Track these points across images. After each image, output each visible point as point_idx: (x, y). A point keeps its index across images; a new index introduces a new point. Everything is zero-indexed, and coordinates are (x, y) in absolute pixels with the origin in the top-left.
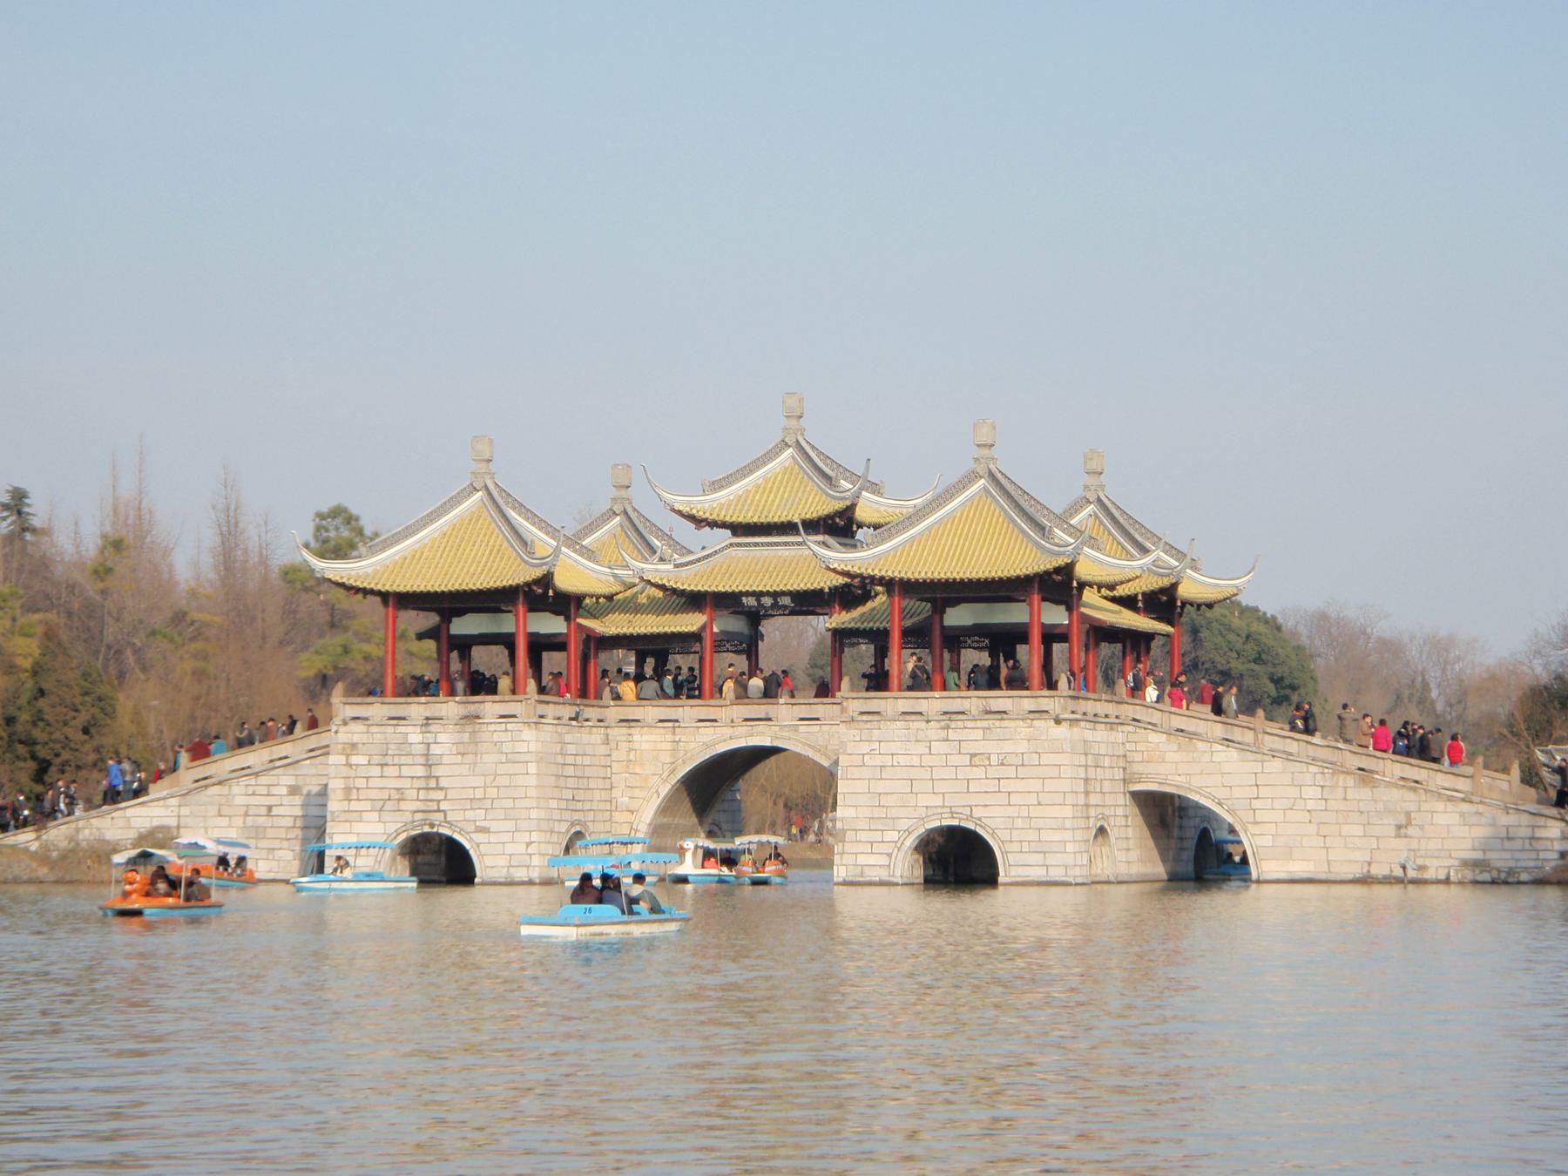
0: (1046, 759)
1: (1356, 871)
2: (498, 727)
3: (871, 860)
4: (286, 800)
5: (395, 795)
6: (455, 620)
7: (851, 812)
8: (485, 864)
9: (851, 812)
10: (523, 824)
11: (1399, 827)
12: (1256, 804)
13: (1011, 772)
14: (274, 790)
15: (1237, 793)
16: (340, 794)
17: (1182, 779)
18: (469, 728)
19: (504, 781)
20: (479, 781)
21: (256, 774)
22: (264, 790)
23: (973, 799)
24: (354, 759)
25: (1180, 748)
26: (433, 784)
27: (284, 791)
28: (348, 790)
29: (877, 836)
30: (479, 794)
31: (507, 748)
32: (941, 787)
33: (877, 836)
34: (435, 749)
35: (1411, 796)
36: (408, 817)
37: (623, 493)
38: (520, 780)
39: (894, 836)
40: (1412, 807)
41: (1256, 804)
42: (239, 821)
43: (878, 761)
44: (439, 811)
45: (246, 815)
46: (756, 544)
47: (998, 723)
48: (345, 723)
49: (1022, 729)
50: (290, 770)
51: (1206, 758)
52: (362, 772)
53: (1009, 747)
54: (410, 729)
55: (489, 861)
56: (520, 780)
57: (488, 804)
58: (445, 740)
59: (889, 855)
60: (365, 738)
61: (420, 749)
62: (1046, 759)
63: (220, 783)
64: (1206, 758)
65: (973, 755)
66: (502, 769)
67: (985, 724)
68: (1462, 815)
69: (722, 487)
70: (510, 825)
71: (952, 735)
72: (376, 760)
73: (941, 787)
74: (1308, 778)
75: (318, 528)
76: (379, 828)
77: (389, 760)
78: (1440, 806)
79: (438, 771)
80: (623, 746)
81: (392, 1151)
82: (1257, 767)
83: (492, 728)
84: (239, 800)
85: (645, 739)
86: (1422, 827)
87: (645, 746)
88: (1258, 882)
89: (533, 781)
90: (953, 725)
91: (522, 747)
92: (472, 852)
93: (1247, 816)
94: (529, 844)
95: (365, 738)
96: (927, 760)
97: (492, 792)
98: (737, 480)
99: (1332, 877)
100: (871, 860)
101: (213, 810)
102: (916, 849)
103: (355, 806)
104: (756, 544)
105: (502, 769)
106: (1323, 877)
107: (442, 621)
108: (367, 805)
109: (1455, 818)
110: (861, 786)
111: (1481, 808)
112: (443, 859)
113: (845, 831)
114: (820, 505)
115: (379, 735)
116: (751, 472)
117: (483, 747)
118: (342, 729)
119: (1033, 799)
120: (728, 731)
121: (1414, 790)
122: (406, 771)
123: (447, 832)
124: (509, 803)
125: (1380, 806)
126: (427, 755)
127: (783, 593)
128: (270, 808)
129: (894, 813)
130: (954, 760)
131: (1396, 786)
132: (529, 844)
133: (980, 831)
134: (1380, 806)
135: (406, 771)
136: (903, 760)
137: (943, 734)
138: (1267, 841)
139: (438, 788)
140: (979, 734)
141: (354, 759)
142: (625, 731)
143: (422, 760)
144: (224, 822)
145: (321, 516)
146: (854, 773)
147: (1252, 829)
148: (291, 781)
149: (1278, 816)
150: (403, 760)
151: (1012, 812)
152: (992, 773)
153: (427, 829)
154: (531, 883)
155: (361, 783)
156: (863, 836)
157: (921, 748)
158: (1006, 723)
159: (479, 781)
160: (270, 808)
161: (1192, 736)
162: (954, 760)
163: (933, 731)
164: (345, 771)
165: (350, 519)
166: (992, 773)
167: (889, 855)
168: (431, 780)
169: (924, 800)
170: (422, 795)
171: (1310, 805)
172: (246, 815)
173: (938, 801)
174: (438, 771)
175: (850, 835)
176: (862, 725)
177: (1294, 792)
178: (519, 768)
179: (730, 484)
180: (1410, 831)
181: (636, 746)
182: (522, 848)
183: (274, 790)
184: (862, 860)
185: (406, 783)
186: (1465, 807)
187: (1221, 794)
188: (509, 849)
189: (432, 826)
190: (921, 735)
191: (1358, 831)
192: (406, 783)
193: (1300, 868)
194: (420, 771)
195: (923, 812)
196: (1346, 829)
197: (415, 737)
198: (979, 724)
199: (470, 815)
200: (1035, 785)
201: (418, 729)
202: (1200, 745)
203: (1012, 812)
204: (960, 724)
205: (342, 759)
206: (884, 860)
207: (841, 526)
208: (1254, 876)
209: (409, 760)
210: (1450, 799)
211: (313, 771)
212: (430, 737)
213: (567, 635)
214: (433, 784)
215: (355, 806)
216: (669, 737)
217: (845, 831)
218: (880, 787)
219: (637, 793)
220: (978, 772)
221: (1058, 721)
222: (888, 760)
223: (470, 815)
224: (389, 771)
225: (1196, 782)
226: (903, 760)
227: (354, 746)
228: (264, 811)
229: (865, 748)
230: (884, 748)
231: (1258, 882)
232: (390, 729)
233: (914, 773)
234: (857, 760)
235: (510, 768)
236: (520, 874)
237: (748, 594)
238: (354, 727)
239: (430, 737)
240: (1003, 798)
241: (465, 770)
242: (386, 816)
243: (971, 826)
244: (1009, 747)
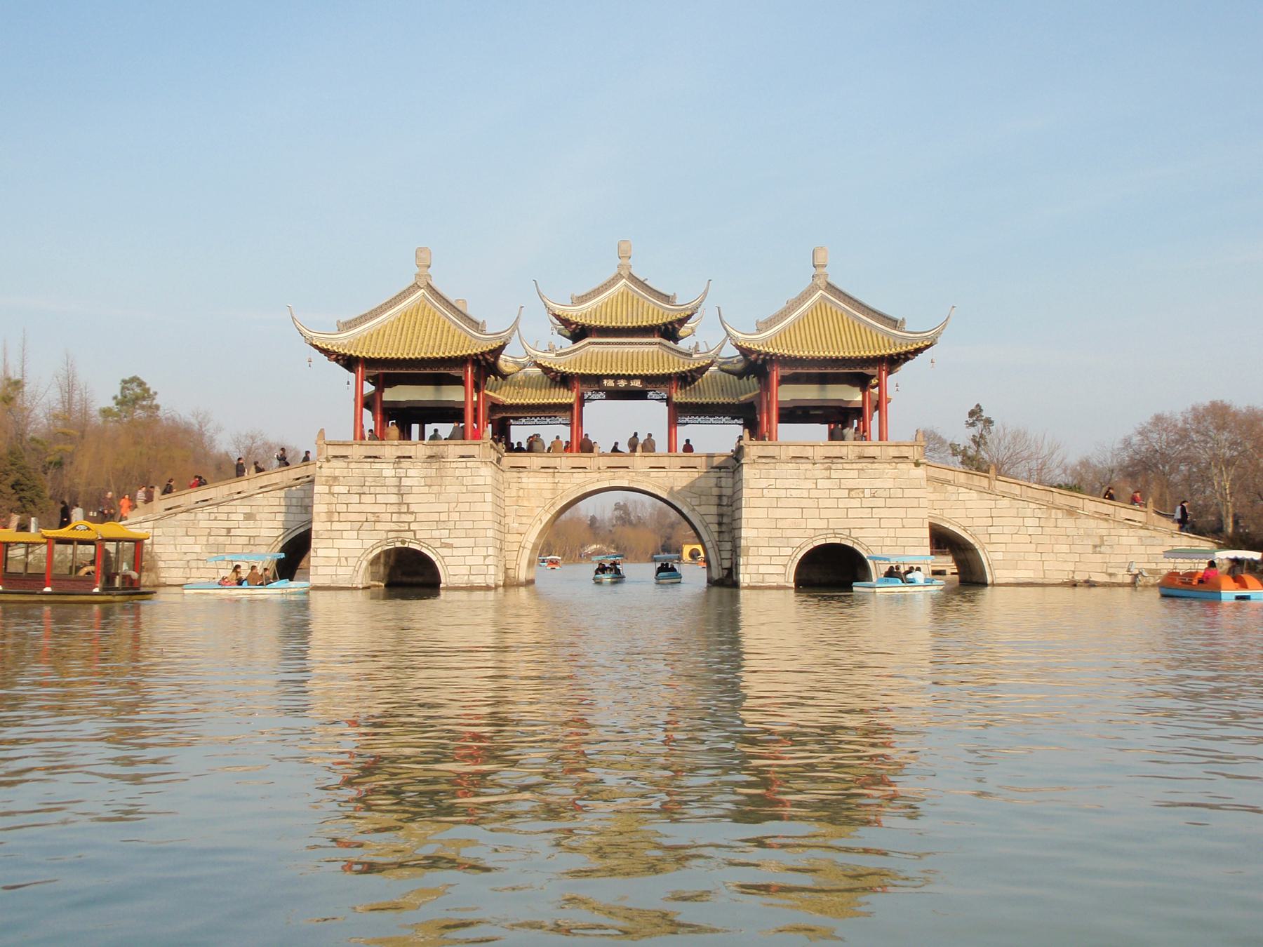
0: (908, 493)
1: (1064, 577)
2: (460, 465)
3: (771, 569)
4: (242, 524)
5: (371, 518)
6: (386, 390)
7: (753, 533)
8: (450, 571)
9: (753, 533)
10: (481, 541)
11: (1095, 546)
12: (991, 530)
13: (881, 502)
14: (233, 517)
15: (977, 522)
16: (324, 517)
17: (937, 512)
18: (436, 465)
19: (466, 507)
20: (444, 507)
21: (218, 504)
22: (224, 517)
23: (852, 523)
24: (336, 489)
25: (935, 491)
26: (404, 509)
27: (241, 517)
28: (330, 513)
29: (775, 551)
30: (444, 517)
31: (467, 481)
32: (825, 513)
33: (775, 551)
34: (405, 482)
35: (1103, 524)
36: (383, 535)
37: (624, 261)
38: (479, 507)
39: (789, 551)
40: (1104, 532)
41: (991, 530)
42: (203, 540)
43: (774, 493)
44: (409, 530)
45: (209, 535)
46: (608, 343)
47: (869, 466)
48: (328, 461)
49: (889, 470)
50: (246, 502)
51: (954, 497)
52: (343, 499)
53: (878, 484)
54: (384, 466)
55: (451, 570)
56: (479, 507)
57: (451, 525)
58: (414, 475)
59: (785, 566)
60: (345, 472)
61: (394, 481)
62: (908, 493)
63: (187, 511)
64: (954, 497)
65: (851, 490)
66: (462, 498)
67: (859, 466)
68: (1140, 538)
69: (586, 301)
70: (471, 542)
71: (834, 474)
72: (355, 489)
73: (825, 513)
74: (1029, 512)
75: (123, 388)
76: (358, 544)
77: (366, 490)
78: (1124, 532)
79: (407, 499)
80: (514, 486)
81: (40, 670)
82: (992, 504)
83: (454, 465)
84: (203, 524)
85: (529, 480)
86: (1111, 546)
87: (531, 486)
88: (993, 585)
89: (489, 507)
90: (834, 466)
91: (480, 481)
92: (438, 564)
93: (985, 539)
94: (485, 557)
95: (345, 472)
96: (814, 493)
97: (455, 516)
98: (595, 297)
99: (1046, 581)
100: (771, 569)
101: (181, 531)
102: (374, 562)
103: (336, 526)
104: (608, 343)
105: (462, 498)
106: (1040, 581)
107: (377, 390)
108: (348, 526)
109: (1135, 541)
110: (762, 513)
111: (1154, 533)
112: (382, 569)
113: (748, 547)
114: (657, 315)
115: (357, 470)
116: (603, 292)
117: (447, 481)
118: (325, 465)
119: (898, 523)
120: (596, 475)
121: (1106, 520)
122: (380, 499)
123: (417, 547)
124: (469, 525)
125: (1082, 532)
126: (399, 486)
127: (635, 377)
128: (229, 530)
129: (788, 533)
130: (836, 493)
131: (1094, 518)
132: (485, 557)
133: (856, 547)
134: (1082, 532)
135: (380, 499)
136: (795, 493)
137: (826, 473)
138: (999, 556)
139: (408, 512)
140: (854, 474)
141: (336, 489)
142: (515, 474)
143: (395, 490)
144: (191, 540)
145: (125, 382)
146: (754, 502)
147: (989, 548)
148: (248, 510)
149: (1006, 538)
150: (378, 490)
151: (883, 533)
152: (866, 503)
153: (399, 545)
154: (487, 588)
155: (342, 508)
156: (764, 551)
157: (810, 484)
158: (876, 466)
159: (444, 507)
160: (229, 530)
161: (943, 482)
162: (836, 493)
163: (818, 471)
164: (327, 498)
165: (141, 384)
166: (866, 503)
167: (785, 566)
168: (403, 505)
169: (812, 524)
170: (395, 518)
171: (1031, 531)
172: (209, 535)
173: (823, 524)
174: (407, 499)
175: (752, 551)
176: (761, 466)
177: (1019, 522)
178: (477, 497)
179: (590, 299)
180: (1103, 549)
181: (524, 485)
182: (480, 561)
183: (233, 517)
184: (762, 569)
185: (382, 508)
186: (1142, 532)
187: (966, 523)
188: (469, 561)
189: (403, 542)
190: (809, 474)
191: (1065, 548)
192: (382, 508)
193: (1024, 575)
194: (394, 499)
195: (812, 533)
196: (1057, 548)
197: (389, 472)
198: (855, 466)
199: (436, 534)
200: (901, 513)
201: (391, 466)
202: (949, 488)
203: (883, 533)
204: (839, 466)
205: (326, 489)
206: (781, 570)
207: (669, 332)
208: (989, 581)
209: (384, 490)
210: (1131, 527)
211: (265, 503)
212: (401, 473)
213: (465, 403)
214: (404, 509)
215: (336, 526)
216: (550, 480)
217: (748, 547)
218: (778, 513)
219: (524, 520)
220: (856, 503)
221: (917, 464)
222: (782, 493)
223: (436, 534)
224: (365, 499)
225: (947, 514)
226: (795, 493)
227: (336, 478)
228: (224, 532)
229: (764, 483)
230: (779, 483)
231: (993, 585)
232: (368, 465)
233: (805, 503)
234: (759, 493)
235: (469, 497)
236: (479, 581)
237: (608, 377)
238: (335, 463)
239: (401, 473)
240: (875, 523)
241: (432, 498)
242: (363, 535)
243: (849, 544)
244: (878, 484)
